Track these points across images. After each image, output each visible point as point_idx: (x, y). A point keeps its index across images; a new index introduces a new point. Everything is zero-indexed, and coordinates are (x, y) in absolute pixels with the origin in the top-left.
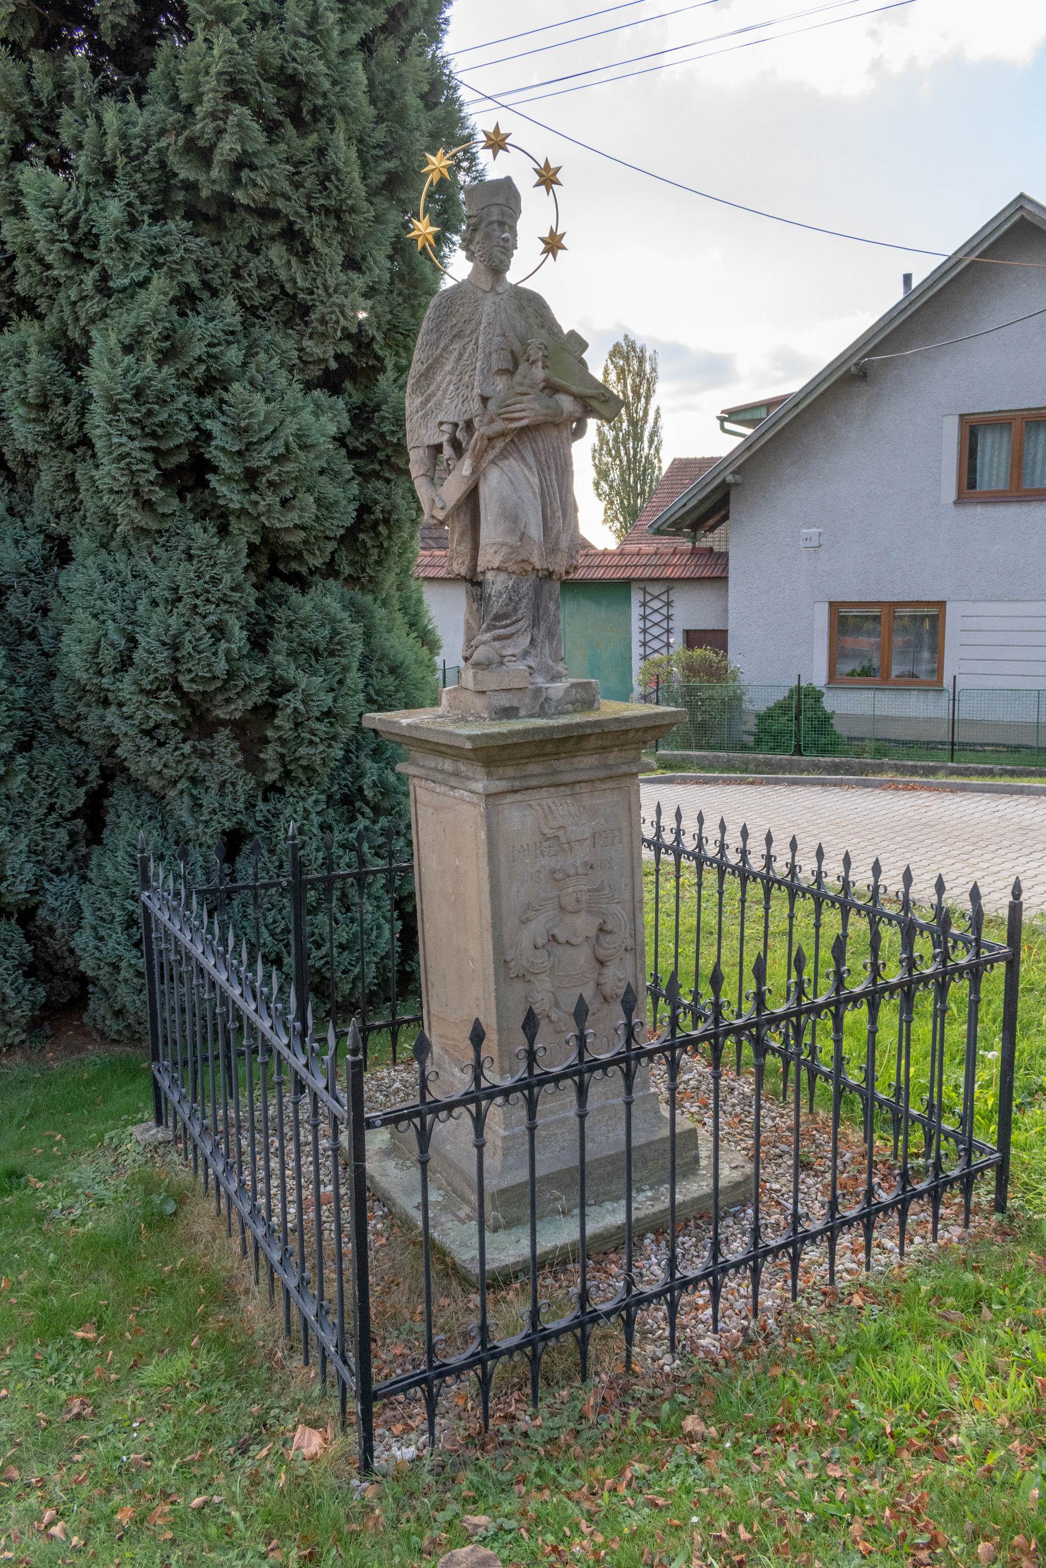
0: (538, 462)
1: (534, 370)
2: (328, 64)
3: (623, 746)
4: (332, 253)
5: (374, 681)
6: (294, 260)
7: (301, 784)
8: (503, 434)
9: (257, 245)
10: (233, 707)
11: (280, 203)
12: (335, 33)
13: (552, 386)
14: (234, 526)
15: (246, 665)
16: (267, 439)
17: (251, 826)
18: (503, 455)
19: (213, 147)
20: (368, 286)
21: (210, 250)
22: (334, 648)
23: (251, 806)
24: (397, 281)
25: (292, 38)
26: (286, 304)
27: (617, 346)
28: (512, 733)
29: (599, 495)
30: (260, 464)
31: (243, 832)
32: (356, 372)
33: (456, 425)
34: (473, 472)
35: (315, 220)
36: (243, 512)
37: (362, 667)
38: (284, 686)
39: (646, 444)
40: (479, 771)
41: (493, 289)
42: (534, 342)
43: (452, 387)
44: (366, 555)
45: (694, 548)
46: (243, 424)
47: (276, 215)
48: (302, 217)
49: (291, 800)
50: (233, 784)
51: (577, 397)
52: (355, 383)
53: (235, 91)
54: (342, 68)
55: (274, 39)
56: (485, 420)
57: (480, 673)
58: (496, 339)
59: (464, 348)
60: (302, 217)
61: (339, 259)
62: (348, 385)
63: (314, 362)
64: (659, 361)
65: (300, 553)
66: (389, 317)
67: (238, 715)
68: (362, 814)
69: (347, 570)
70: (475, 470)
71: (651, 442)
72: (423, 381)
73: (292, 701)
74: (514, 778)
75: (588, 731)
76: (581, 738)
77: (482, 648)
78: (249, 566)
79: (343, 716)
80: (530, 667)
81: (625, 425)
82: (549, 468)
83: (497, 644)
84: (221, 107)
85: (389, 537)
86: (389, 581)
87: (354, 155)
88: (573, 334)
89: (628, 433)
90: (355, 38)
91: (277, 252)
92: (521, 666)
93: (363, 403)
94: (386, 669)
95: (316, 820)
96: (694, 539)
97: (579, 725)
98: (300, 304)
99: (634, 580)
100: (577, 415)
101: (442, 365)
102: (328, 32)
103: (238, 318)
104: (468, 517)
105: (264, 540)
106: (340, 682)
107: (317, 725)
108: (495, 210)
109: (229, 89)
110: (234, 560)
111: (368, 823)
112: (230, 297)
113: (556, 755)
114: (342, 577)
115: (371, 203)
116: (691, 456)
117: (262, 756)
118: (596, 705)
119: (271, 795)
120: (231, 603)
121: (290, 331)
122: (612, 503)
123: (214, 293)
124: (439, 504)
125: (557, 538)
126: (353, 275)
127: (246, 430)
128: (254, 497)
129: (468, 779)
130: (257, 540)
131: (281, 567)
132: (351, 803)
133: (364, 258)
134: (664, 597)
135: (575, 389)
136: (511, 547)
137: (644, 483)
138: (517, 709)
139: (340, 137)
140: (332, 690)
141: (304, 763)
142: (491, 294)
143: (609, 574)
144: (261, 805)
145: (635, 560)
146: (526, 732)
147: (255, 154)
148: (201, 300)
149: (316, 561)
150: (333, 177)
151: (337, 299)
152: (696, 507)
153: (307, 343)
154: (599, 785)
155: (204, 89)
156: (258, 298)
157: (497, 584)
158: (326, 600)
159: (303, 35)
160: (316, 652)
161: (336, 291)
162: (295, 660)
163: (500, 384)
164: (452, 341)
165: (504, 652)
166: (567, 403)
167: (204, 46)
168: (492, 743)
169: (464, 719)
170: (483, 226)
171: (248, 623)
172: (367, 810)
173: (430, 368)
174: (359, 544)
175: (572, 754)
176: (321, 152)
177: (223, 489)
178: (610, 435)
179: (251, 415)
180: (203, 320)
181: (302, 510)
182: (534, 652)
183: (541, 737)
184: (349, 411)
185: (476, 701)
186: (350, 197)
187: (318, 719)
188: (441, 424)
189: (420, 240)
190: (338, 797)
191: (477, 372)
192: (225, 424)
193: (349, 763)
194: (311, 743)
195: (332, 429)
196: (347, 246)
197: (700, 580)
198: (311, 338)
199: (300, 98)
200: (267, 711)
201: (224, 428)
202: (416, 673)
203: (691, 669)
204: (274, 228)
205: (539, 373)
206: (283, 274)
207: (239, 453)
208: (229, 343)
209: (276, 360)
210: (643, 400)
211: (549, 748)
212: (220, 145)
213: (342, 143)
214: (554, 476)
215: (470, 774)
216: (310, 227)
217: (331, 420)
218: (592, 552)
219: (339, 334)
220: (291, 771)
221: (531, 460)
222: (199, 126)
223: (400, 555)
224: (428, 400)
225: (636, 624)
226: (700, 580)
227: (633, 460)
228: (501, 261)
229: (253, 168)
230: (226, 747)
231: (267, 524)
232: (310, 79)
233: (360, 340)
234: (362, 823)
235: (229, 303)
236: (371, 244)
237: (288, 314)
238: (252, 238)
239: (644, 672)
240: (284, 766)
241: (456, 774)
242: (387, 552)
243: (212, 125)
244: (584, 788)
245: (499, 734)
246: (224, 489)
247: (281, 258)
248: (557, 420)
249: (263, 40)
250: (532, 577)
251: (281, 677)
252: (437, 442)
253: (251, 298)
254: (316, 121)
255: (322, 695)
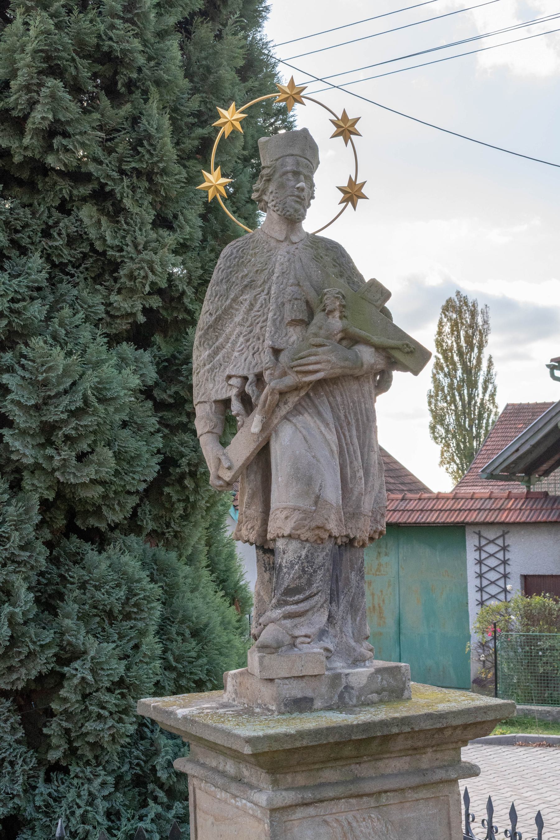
0: (337, 418)
1: (331, 320)
2: (145, 43)
3: (438, 746)
4: (142, 211)
5: (173, 646)
6: (104, 220)
7: (88, 763)
8: (296, 388)
9: (69, 207)
10: (15, 676)
11: (92, 167)
12: (152, 15)
13: (349, 334)
14: (28, 482)
15: (32, 630)
16: (66, 392)
17: (29, 812)
18: (297, 410)
19: (26, 117)
20: (178, 243)
21: (21, 211)
22: (130, 610)
23: (30, 788)
24: (209, 238)
25: (109, 19)
26: (96, 261)
27: (449, 301)
28: (301, 734)
29: (435, 438)
30: (56, 418)
31: (20, 819)
32: (162, 326)
33: (246, 379)
34: (263, 430)
35: (126, 181)
36: (36, 468)
37: (161, 631)
38: (73, 653)
39: (480, 389)
40: (260, 777)
41: (286, 238)
42: (330, 291)
43: (241, 339)
44: (171, 510)
45: (528, 492)
46: (40, 378)
47: (88, 177)
48: (113, 180)
49: (75, 782)
50: (12, 764)
51: (379, 348)
52: (165, 337)
53: (50, 67)
54: (157, 46)
55: (91, 21)
56: (277, 373)
57: (268, 657)
58: (289, 289)
59: (255, 299)
60: (113, 180)
61: (150, 218)
62: (158, 338)
63: (122, 317)
64: (490, 314)
65: (99, 507)
66: (200, 272)
67: (20, 686)
68: (155, 799)
69: (149, 525)
70: (265, 427)
71: (485, 389)
72: (211, 334)
73: (79, 671)
74: (304, 788)
75: (395, 730)
76: (387, 739)
77: (271, 627)
78: (43, 522)
79: (136, 687)
80: (327, 650)
81: (459, 373)
82: (349, 424)
83: (288, 623)
84: (35, 81)
85: (196, 491)
86: (196, 536)
87: (166, 122)
88: (374, 283)
89: (462, 380)
90: (171, 20)
91: (87, 213)
92: (317, 649)
93: (173, 356)
94: (187, 632)
95: (102, 806)
96: (529, 483)
97: (383, 723)
98: (109, 260)
99: (468, 524)
100: (380, 367)
101: (232, 316)
102: (145, 15)
103: (44, 275)
104: (259, 477)
105: (59, 495)
106: (136, 647)
107: (106, 697)
108: (290, 161)
109: (45, 65)
110: (24, 517)
111: (159, 809)
112: (38, 254)
113: (357, 759)
114: (145, 533)
115: (185, 167)
116: (524, 401)
117: (45, 731)
118: (406, 693)
119: (53, 775)
120: (19, 563)
121: (98, 287)
122: (448, 446)
123: (23, 251)
124: (225, 464)
125: (359, 500)
126: (163, 232)
127: (45, 384)
128: (50, 451)
129: (251, 787)
130: (51, 496)
131: (79, 523)
132: (145, 785)
133: (175, 217)
134: (500, 542)
135: (376, 339)
136: (304, 512)
137: (479, 427)
138: (311, 700)
139: (153, 106)
140: (126, 657)
141: (91, 739)
142: (285, 244)
143: (443, 518)
144: (42, 788)
145: (469, 504)
146: (317, 733)
147: (68, 123)
148: (9, 258)
149: (116, 516)
150: (145, 143)
151: (147, 255)
152: (529, 452)
153: (114, 298)
154: (410, 795)
155: (20, 65)
156: (67, 255)
157: (289, 553)
158: (127, 558)
159: (119, 17)
160: (110, 614)
161: (145, 248)
162: (86, 624)
163: (294, 335)
164: (242, 292)
165: (297, 633)
166: (367, 355)
167: (22, 28)
168: (276, 746)
169: (249, 712)
170: (277, 175)
171: (39, 583)
172: (161, 794)
173: (219, 319)
174: (163, 498)
175: (376, 757)
176: (135, 120)
177: (16, 444)
178: (445, 382)
179: (50, 369)
180: (7, 277)
181: (100, 464)
182: (331, 631)
183: (337, 738)
184: (158, 364)
185: (263, 689)
186: (161, 160)
187: (109, 690)
188: (229, 377)
189: (211, 192)
190: (128, 778)
191: (269, 323)
192: (23, 378)
193: (143, 738)
194: (99, 717)
195: (135, 382)
196: (158, 207)
197: (536, 524)
198: (119, 292)
199: (116, 73)
200: (53, 680)
201: (21, 382)
202: (220, 636)
203: (530, 617)
204: (84, 190)
205: (336, 323)
206: (93, 234)
207: (37, 407)
208: (32, 299)
209: (81, 315)
210: (476, 350)
211: (348, 751)
212: (33, 114)
213: (155, 111)
214: (354, 432)
215: (254, 781)
216: (121, 187)
217: (135, 372)
218: (426, 495)
219: (147, 289)
220: (77, 749)
221: (328, 416)
222: (13, 99)
223: (208, 509)
224: (216, 353)
225: (472, 569)
226: (536, 524)
227: (468, 405)
228: (296, 211)
229: (66, 135)
230: (5, 721)
231: (62, 480)
232: (125, 55)
233: (169, 293)
234: (153, 809)
235: (36, 261)
236: (183, 204)
237: (97, 271)
238: (63, 200)
239: (482, 620)
240: (70, 742)
241: (238, 780)
242: (194, 506)
243: (25, 98)
244: (393, 799)
245: (286, 735)
246: (17, 444)
247: (91, 217)
248: (357, 372)
249: (83, 23)
250: (329, 545)
251: (70, 643)
252: (224, 397)
253: (60, 256)
254: (131, 92)
255: (114, 663)
